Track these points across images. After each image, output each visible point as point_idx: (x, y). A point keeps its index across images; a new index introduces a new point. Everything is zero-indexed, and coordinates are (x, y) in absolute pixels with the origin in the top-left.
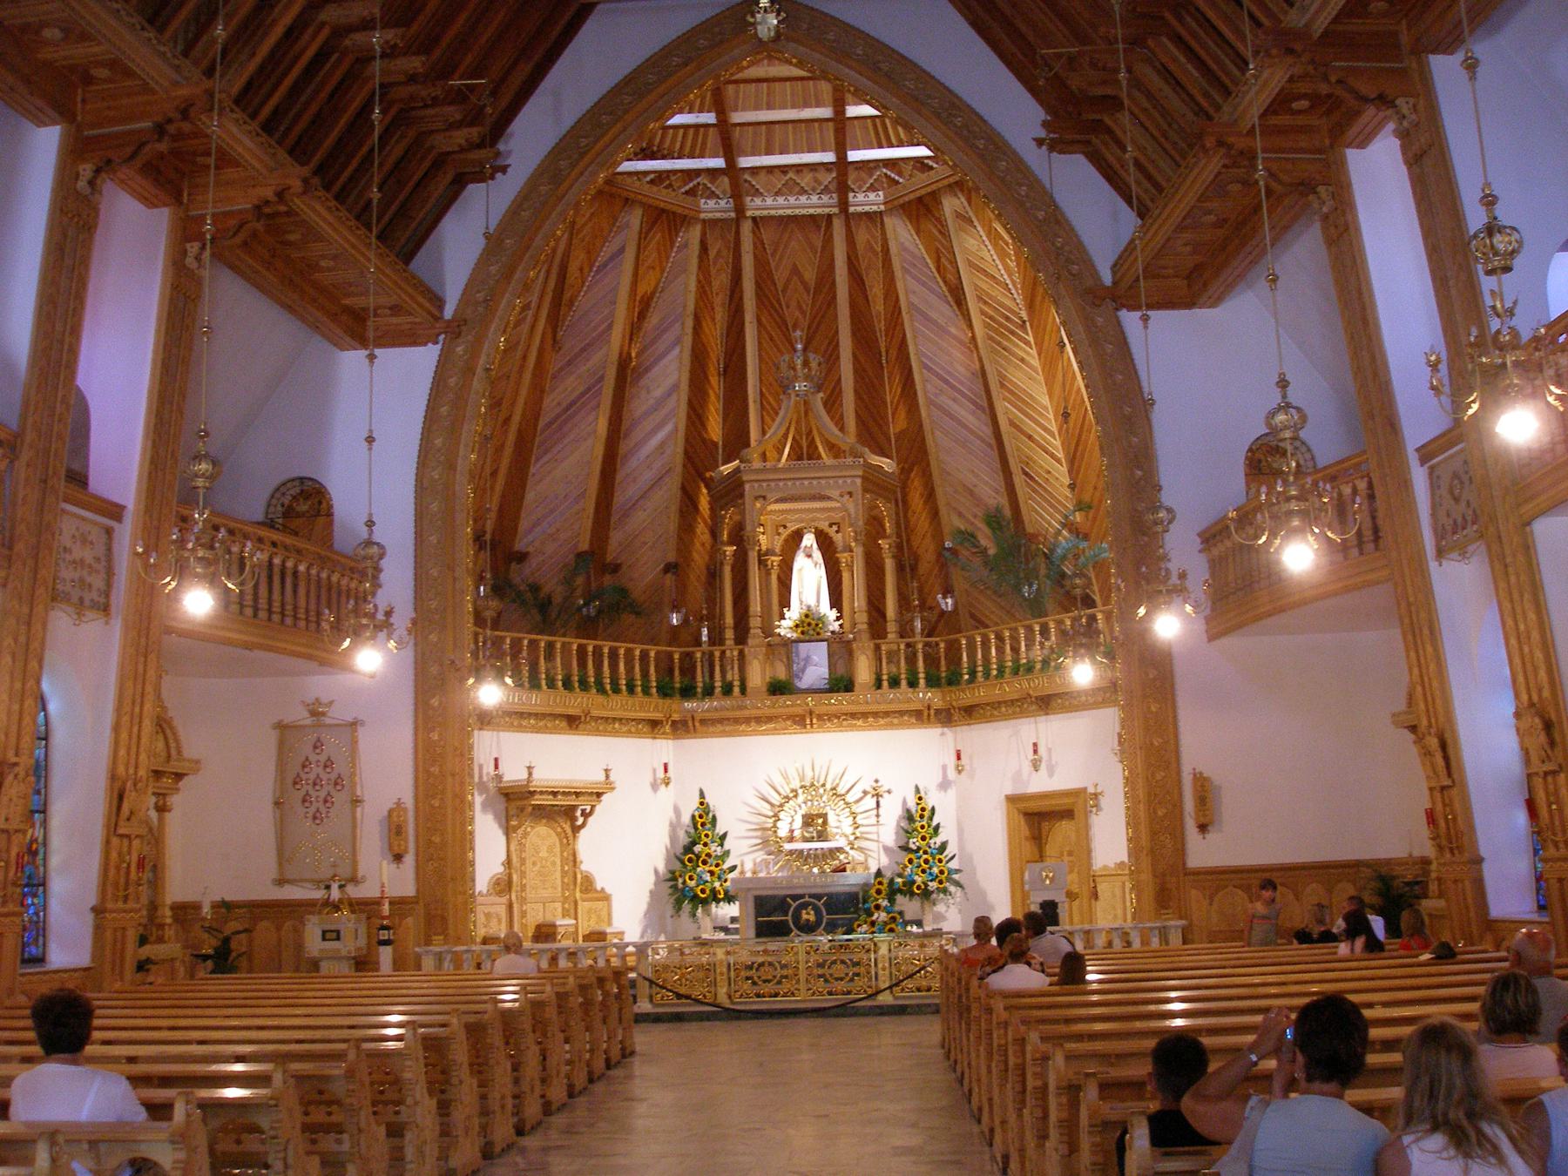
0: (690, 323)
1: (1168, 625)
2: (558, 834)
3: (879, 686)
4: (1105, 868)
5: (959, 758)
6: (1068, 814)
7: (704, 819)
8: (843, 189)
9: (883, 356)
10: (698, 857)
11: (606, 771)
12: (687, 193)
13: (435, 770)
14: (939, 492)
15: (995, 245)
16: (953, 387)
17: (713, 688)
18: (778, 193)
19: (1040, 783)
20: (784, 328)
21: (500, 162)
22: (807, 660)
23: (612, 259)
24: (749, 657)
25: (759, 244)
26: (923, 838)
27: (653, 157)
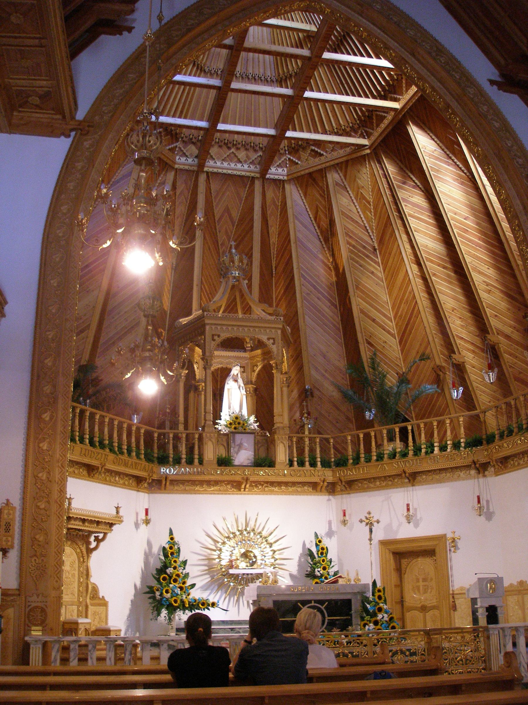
3: (291, 464)
7: (171, 552)
10: (170, 577)
11: (117, 508)
12: (169, 149)
15: (360, 203)
17: (180, 458)
23: (122, 179)
24: (205, 440)
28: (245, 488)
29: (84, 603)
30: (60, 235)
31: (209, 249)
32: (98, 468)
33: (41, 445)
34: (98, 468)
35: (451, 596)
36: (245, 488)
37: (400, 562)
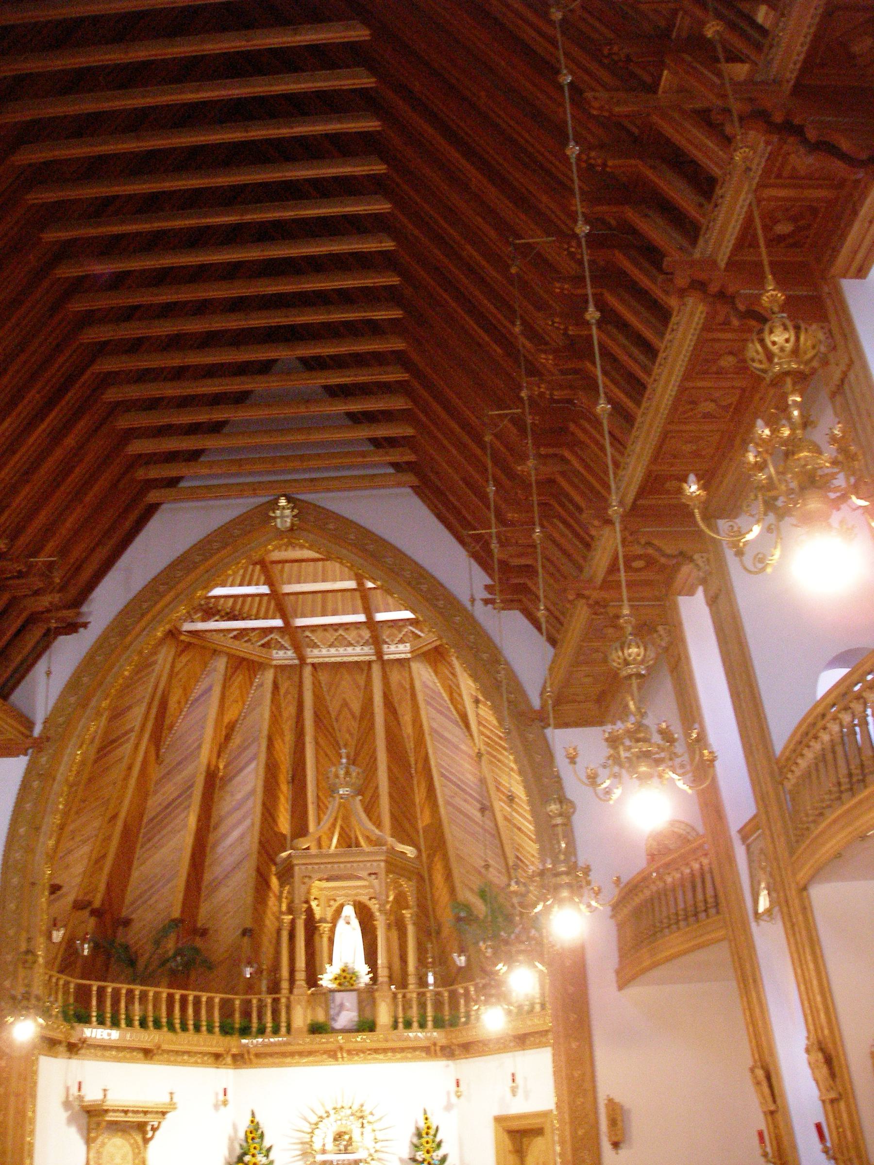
0: (264, 743)
2: (131, 1145)
3: (395, 1026)
7: (255, 1133)
8: (377, 642)
9: (410, 768)
12: (263, 645)
14: (456, 872)
16: (463, 790)
18: (331, 646)
20: (336, 746)
21: (82, 620)
22: (342, 1006)
24: (293, 1004)
25: (317, 685)
26: (428, 1152)
27: (235, 618)
31: (327, 755)
37: (521, 1142)
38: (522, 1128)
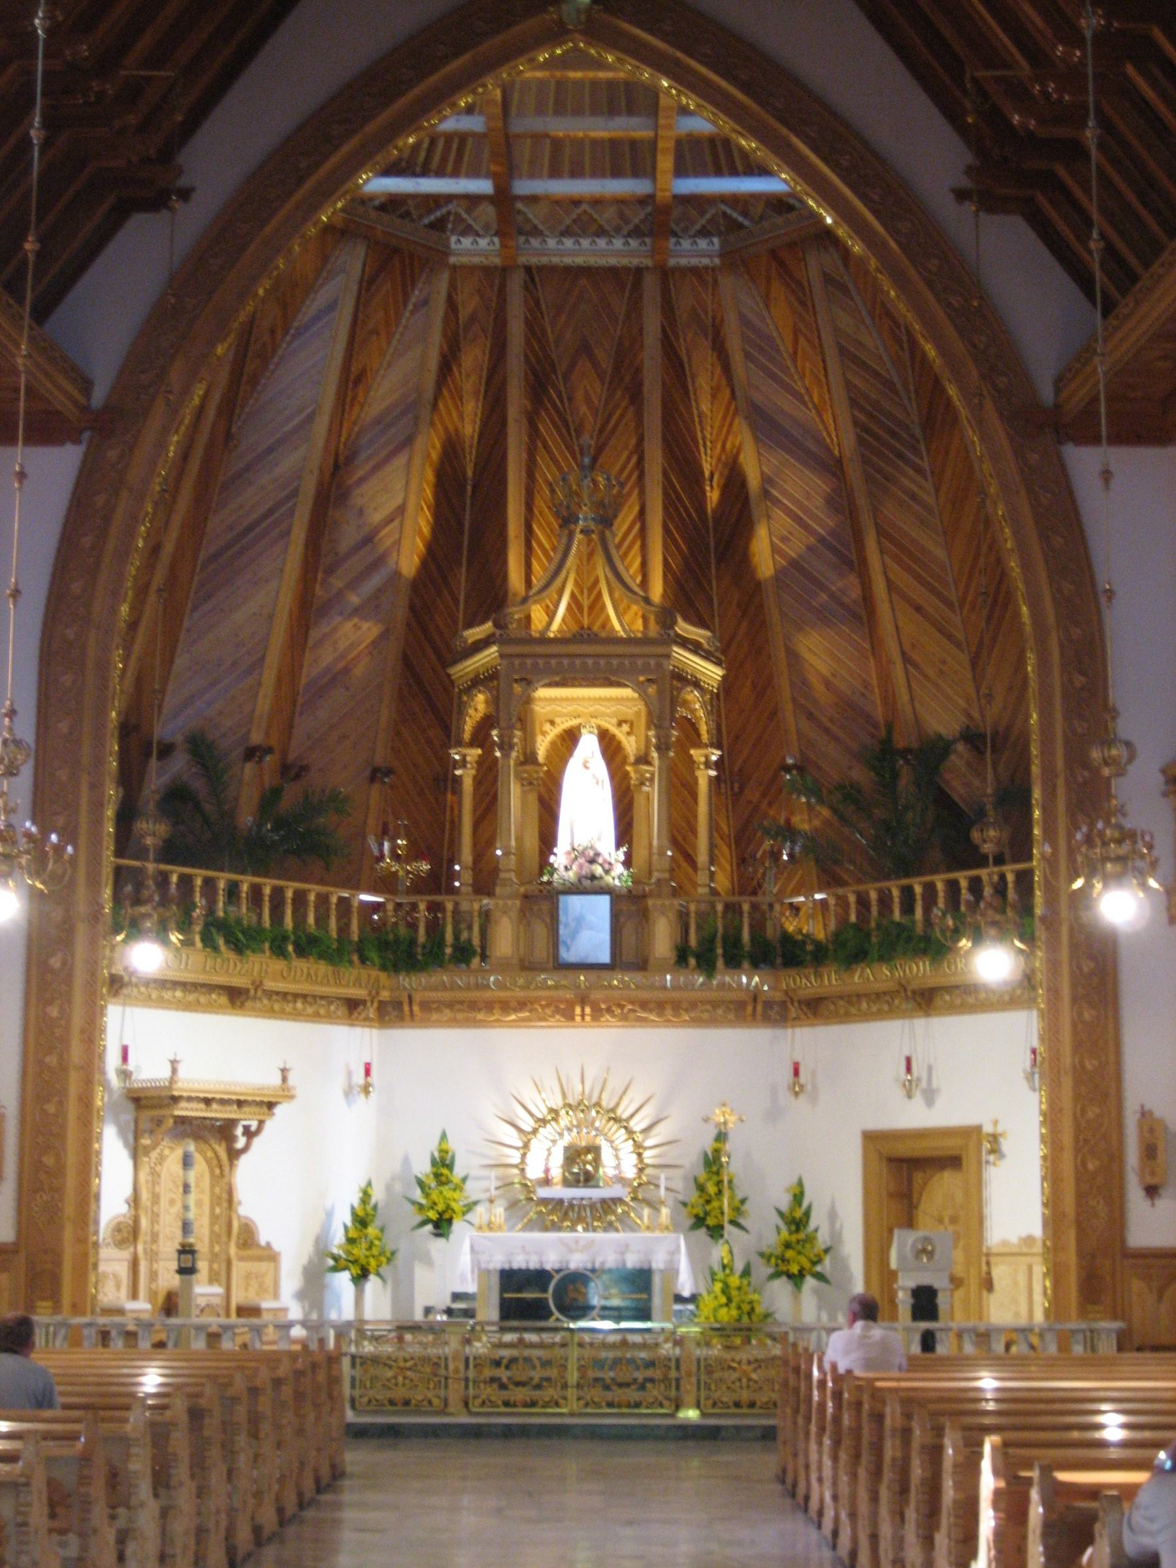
1: (1121, 906)
4: (1005, 1243)
5: (796, 1073)
6: (954, 1162)
11: (284, 1071)
13: (52, 1060)
18: (566, 233)
19: (914, 1117)
22: (580, 920)
23: (316, 318)
28: (583, 1016)
29: (224, 1257)
30: (72, 637)
32: (248, 990)
33: (48, 1010)
34: (248, 990)
35: (984, 1259)
36: (583, 1016)
38: (917, 1154)
